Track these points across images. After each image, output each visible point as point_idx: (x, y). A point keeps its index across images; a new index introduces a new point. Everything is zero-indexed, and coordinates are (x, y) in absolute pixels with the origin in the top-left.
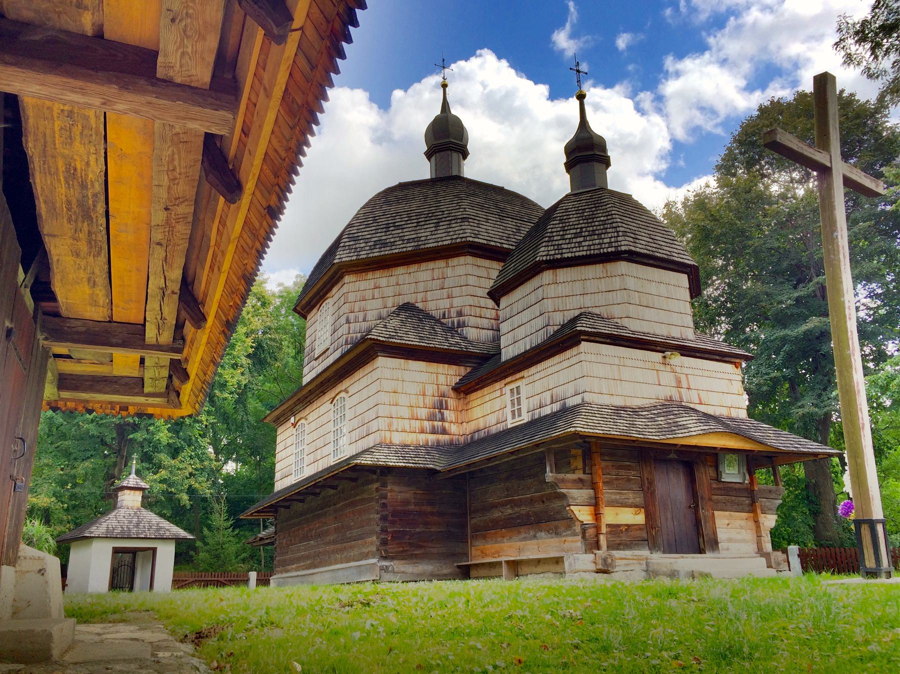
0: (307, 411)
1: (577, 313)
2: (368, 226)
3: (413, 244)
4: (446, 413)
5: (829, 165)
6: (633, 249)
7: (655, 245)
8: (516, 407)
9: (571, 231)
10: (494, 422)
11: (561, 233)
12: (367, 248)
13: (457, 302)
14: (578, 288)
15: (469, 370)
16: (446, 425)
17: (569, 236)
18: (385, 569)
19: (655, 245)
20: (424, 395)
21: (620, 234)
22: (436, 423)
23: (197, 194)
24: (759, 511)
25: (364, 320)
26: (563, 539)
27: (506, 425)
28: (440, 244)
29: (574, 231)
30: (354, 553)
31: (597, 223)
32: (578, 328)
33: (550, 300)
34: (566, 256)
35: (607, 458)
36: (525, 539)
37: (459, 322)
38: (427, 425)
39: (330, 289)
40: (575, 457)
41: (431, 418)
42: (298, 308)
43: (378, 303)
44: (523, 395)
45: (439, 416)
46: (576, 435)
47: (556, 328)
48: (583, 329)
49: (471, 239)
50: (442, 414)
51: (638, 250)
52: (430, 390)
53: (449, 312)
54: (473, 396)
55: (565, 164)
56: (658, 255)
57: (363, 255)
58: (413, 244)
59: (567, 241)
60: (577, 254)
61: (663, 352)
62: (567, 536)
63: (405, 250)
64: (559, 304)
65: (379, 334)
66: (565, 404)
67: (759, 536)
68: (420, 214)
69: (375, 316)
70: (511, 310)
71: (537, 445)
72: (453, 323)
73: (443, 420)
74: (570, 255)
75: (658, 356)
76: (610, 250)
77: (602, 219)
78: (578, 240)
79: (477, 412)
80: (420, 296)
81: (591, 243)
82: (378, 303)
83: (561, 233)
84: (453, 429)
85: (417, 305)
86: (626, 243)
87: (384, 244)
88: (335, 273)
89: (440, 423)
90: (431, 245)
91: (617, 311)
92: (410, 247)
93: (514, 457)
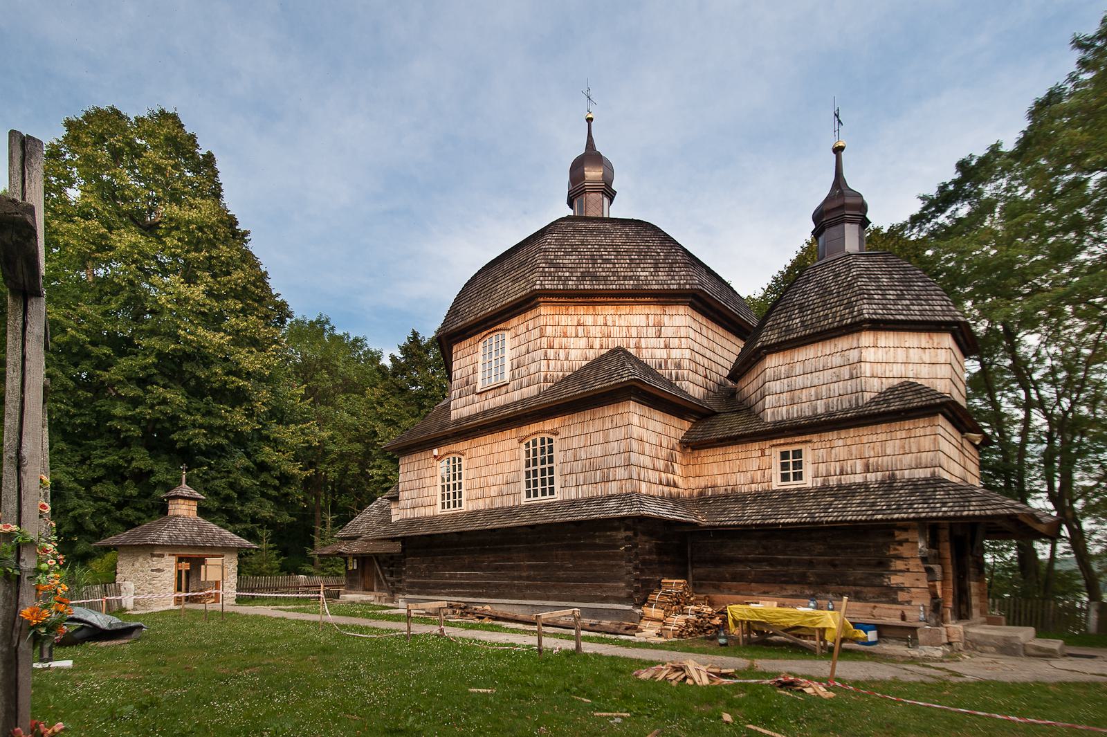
13: (676, 354)
14: (901, 355)
23: (18, 598)
28: (666, 287)
30: (578, 592)
33: (868, 365)
47: (873, 395)
58: (632, 282)
64: (879, 369)
79: (706, 470)
82: (582, 342)
85: (629, 350)
87: (595, 277)
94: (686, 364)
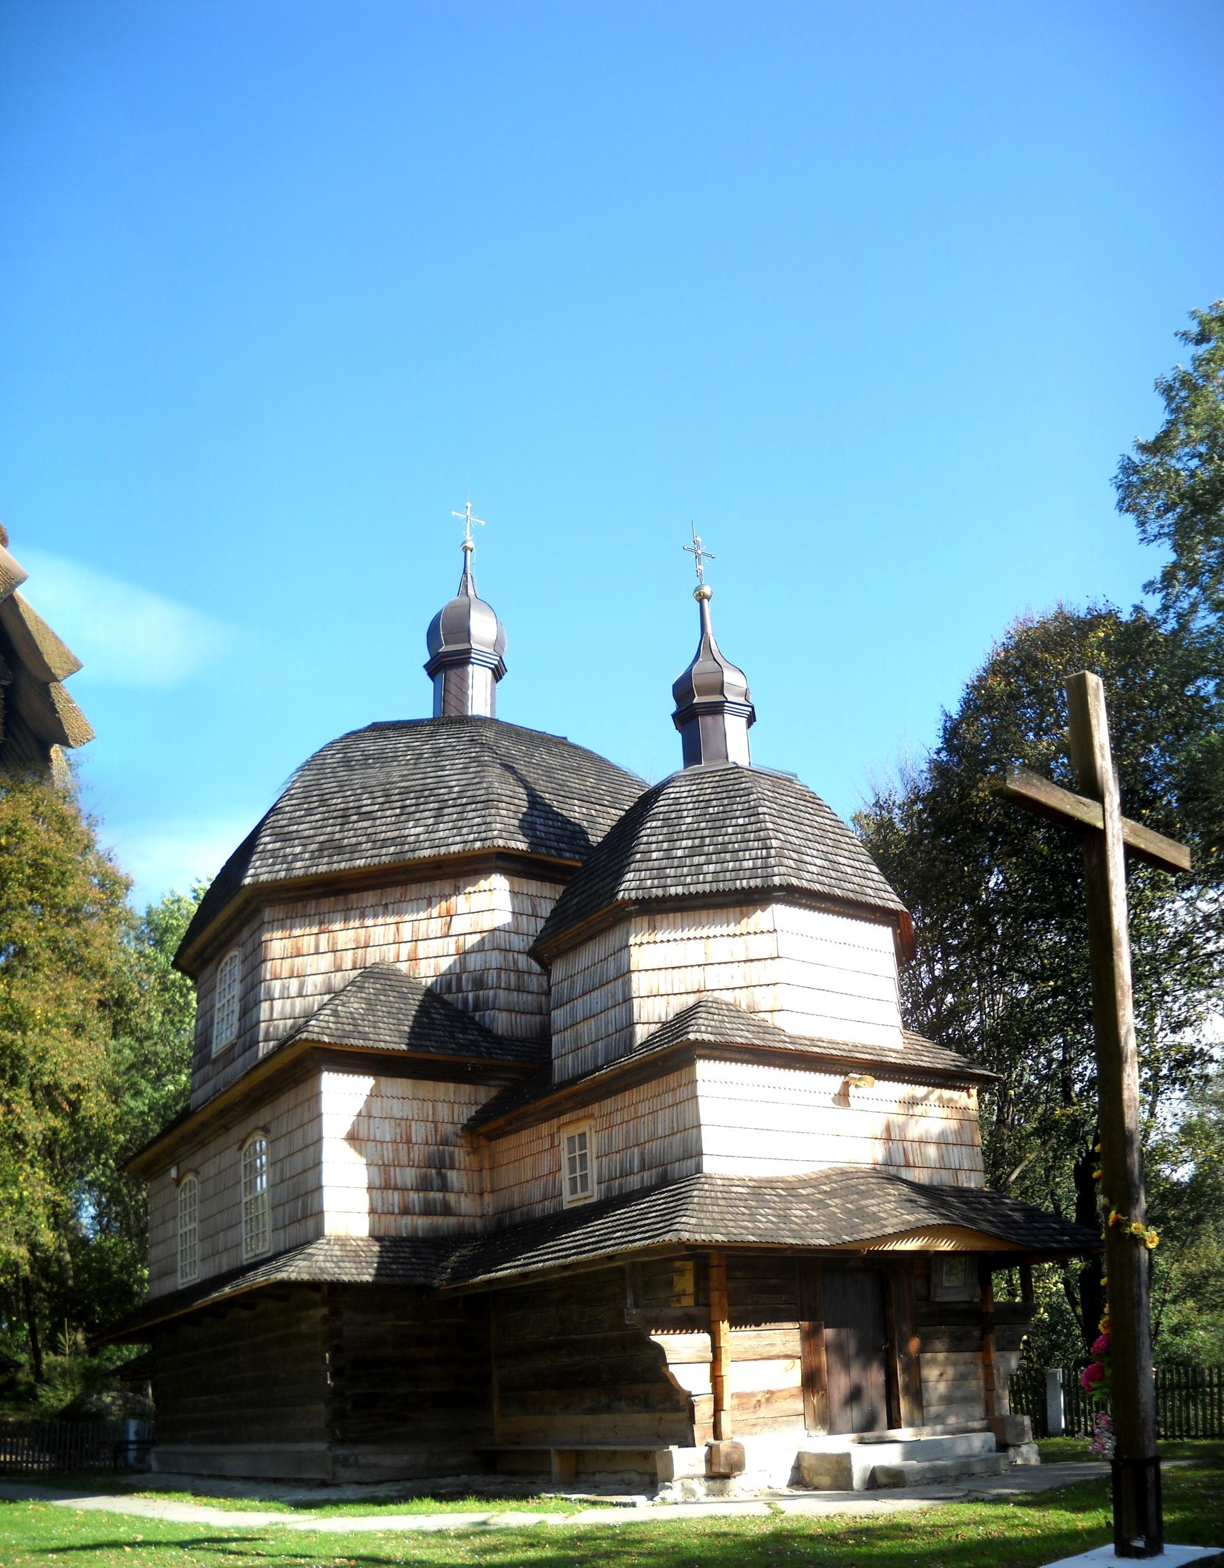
0: (198, 1158)
1: (691, 1000)
2: (309, 811)
3: (392, 849)
4: (452, 1176)
5: (1100, 825)
6: (795, 881)
7: (833, 874)
8: (578, 1173)
9: (684, 843)
10: (537, 1195)
11: (665, 845)
12: (307, 855)
15: (494, 1092)
16: (451, 1198)
17: (680, 853)
18: (345, 1462)
19: (833, 874)
20: (409, 1141)
21: (773, 852)
22: (431, 1194)
24: (992, 1348)
25: (300, 995)
26: (658, 1415)
27: (561, 1204)
28: (443, 850)
29: (690, 843)
31: (730, 830)
32: (691, 1036)
34: (673, 891)
35: (738, 1274)
36: (592, 1411)
37: (477, 998)
38: (415, 1197)
39: (239, 930)
40: (681, 1272)
41: (423, 1185)
42: (183, 962)
43: (325, 962)
44: (592, 1149)
45: (436, 1182)
46: (682, 1244)
48: (698, 1036)
49: (501, 842)
50: (443, 1178)
51: (805, 884)
52: (419, 1132)
53: (459, 979)
54: (505, 1143)
55: (675, 716)
56: (838, 892)
57: (299, 869)
58: (392, 849)
59: (676, 862)
60: (693, 889)
61: (846, 1074)
62: (663, 1410)
63: (376, 860)
65: (322, 1030)
66: (666, 1172)
67: (989, 1388)
68: (406, 791)
69: (320, 988)
70: (572, 987)
71: (610, 1258)
72: (466, 1001)
73: (444, 1187)
74: (680, 890)
75: (834, 1082)
76: (753, 883)
77: (741, 821)
78: (696, 860)
80: (405, 950)
81: (719, 867)
82: (325, 962)
83: (665, 845)
84: (465, 1204)
85: (398, 965)
86: (783, 870)
87: (339, 849)
88: (247, 902)
89: (439, 1195)
90: (427, 853)
91: (763, 999)
92: (387, 855)
93: (566, 1274)
94: (492, 977)
